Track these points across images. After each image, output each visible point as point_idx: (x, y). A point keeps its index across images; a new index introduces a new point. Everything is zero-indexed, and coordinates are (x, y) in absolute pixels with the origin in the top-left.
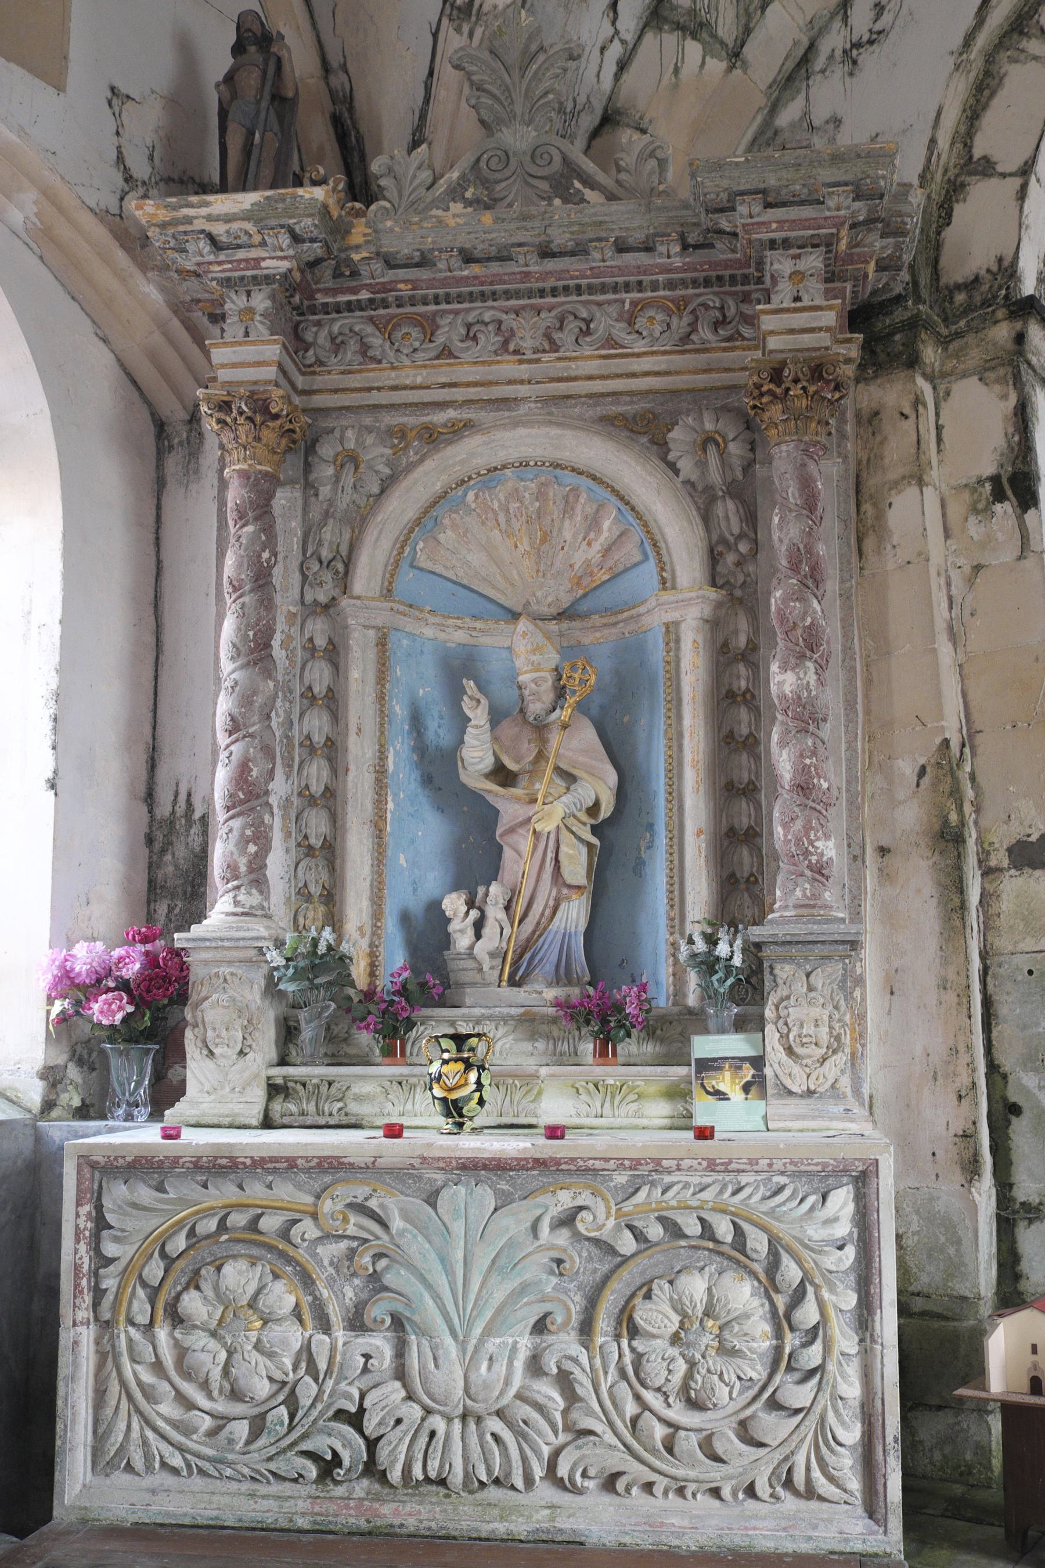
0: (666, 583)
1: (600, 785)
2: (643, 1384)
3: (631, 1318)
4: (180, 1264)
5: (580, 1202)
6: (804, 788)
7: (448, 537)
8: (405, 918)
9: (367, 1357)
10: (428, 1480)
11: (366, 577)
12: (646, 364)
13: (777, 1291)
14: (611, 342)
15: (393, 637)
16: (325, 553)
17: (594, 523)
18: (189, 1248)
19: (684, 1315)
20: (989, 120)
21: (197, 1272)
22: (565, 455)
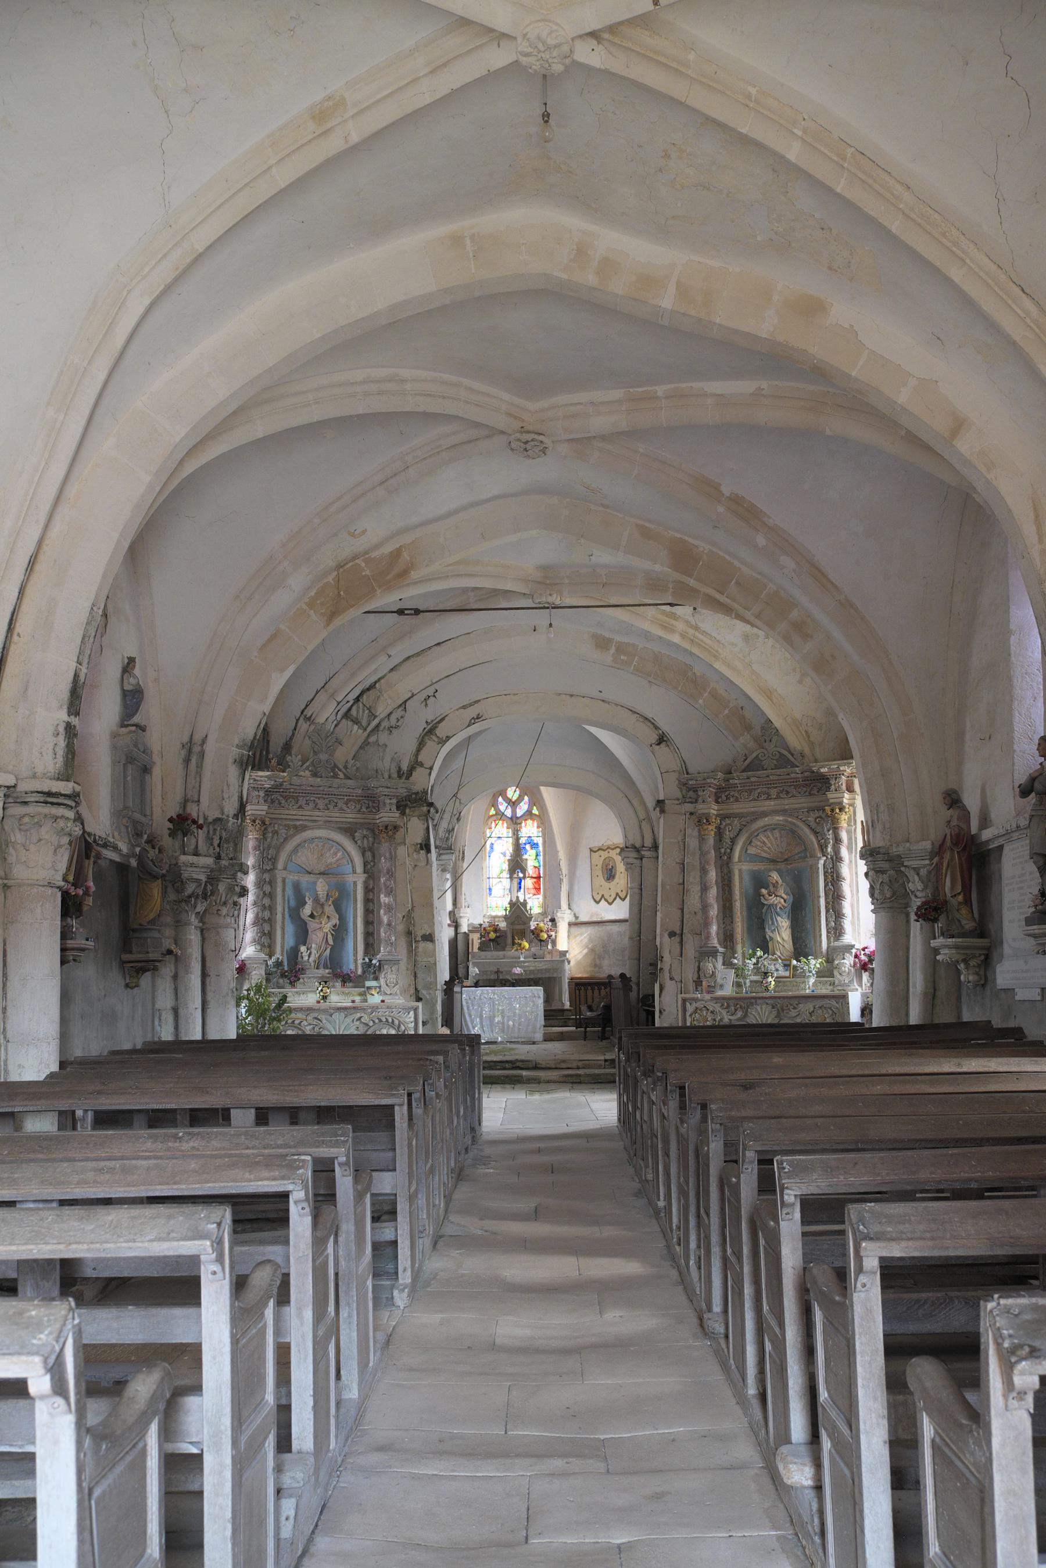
0: (354, 872)
1: (335, 920)
6: (389, 925)
12: (350, 816)
14: (341, 809)
17: (336, 854)
20: (422, 752)
22: (330, 837)
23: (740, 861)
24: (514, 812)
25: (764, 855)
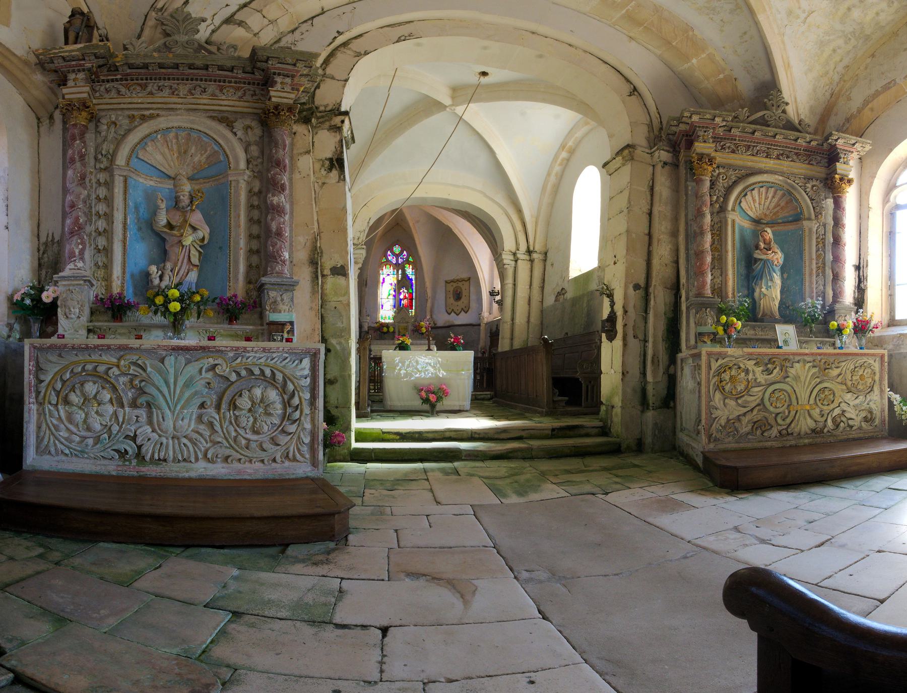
1: (204, 231)
2: (238, 426)
3: (234, 403)
4: (68, 383)
5: (216, 362)
7: (149, 148)
8: (132, 276)
9: (137, 417)
10: (159, 459)
11: (121, 160)
13: (285, 393)
15: (129, 180)
16: (104, 152)
18: (71, 377)
19: (253, 402)
21: (74, 386)
23: (733, 210)
24: (397, 260)
25: (750, 213)
